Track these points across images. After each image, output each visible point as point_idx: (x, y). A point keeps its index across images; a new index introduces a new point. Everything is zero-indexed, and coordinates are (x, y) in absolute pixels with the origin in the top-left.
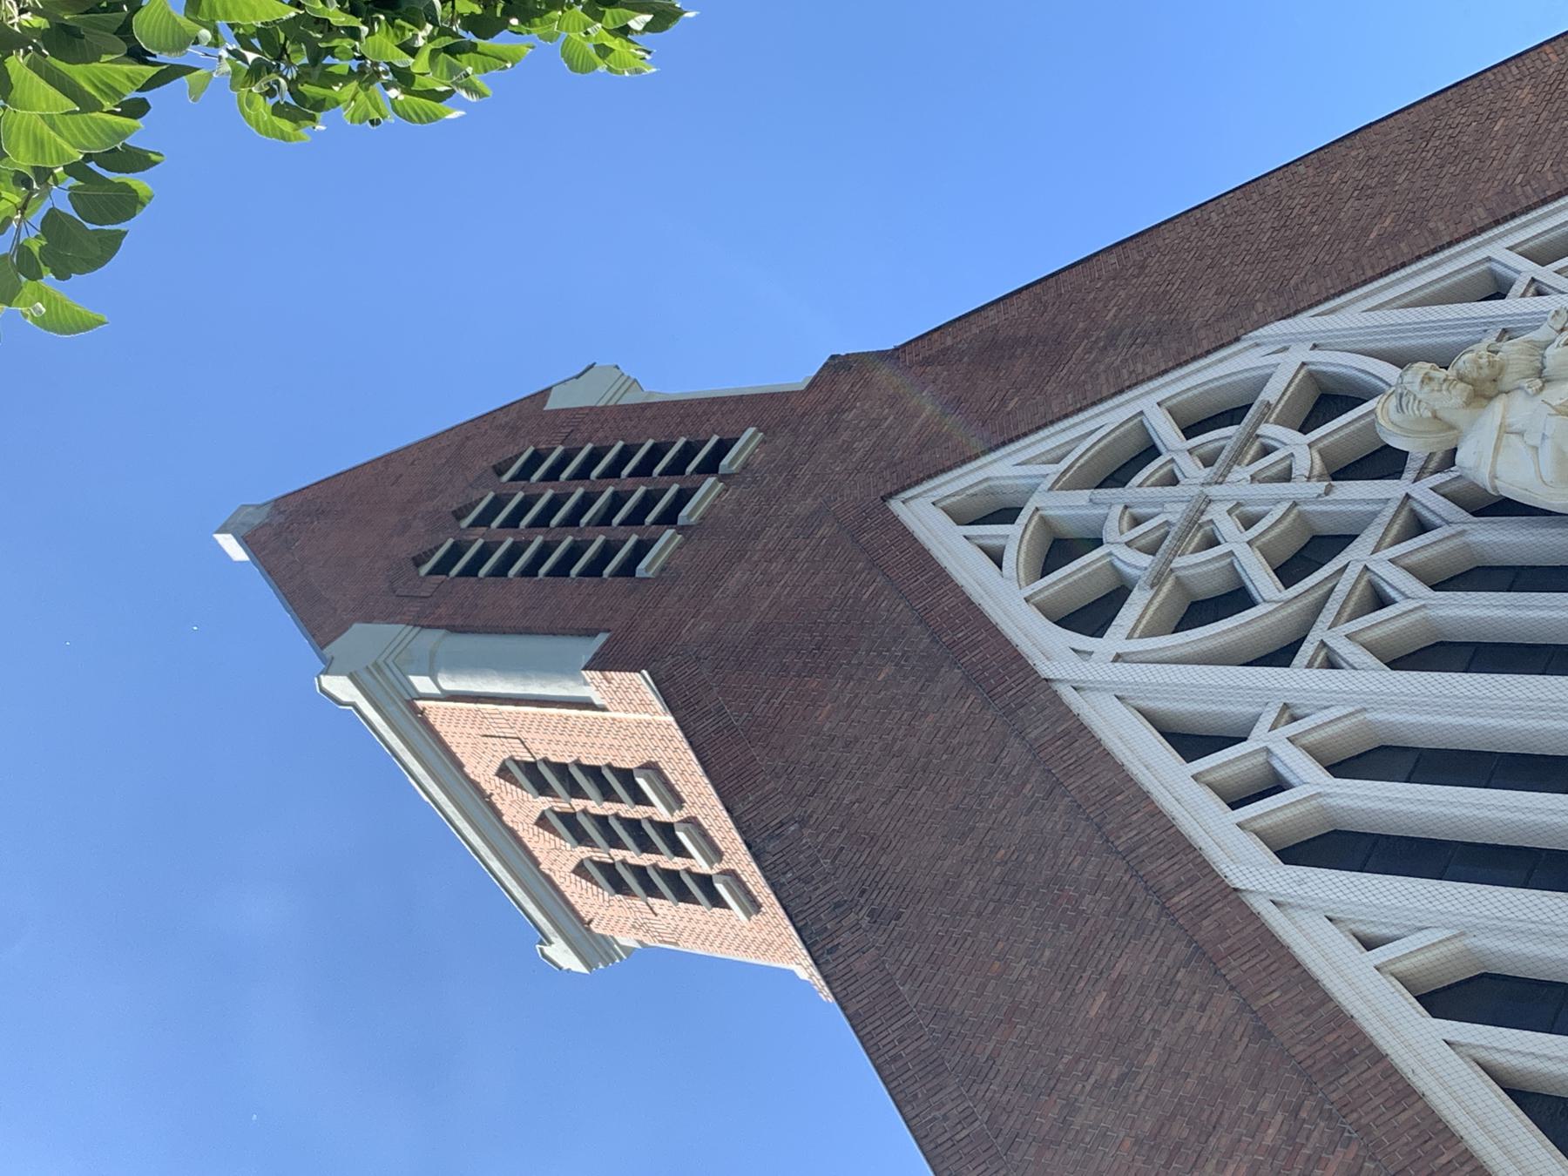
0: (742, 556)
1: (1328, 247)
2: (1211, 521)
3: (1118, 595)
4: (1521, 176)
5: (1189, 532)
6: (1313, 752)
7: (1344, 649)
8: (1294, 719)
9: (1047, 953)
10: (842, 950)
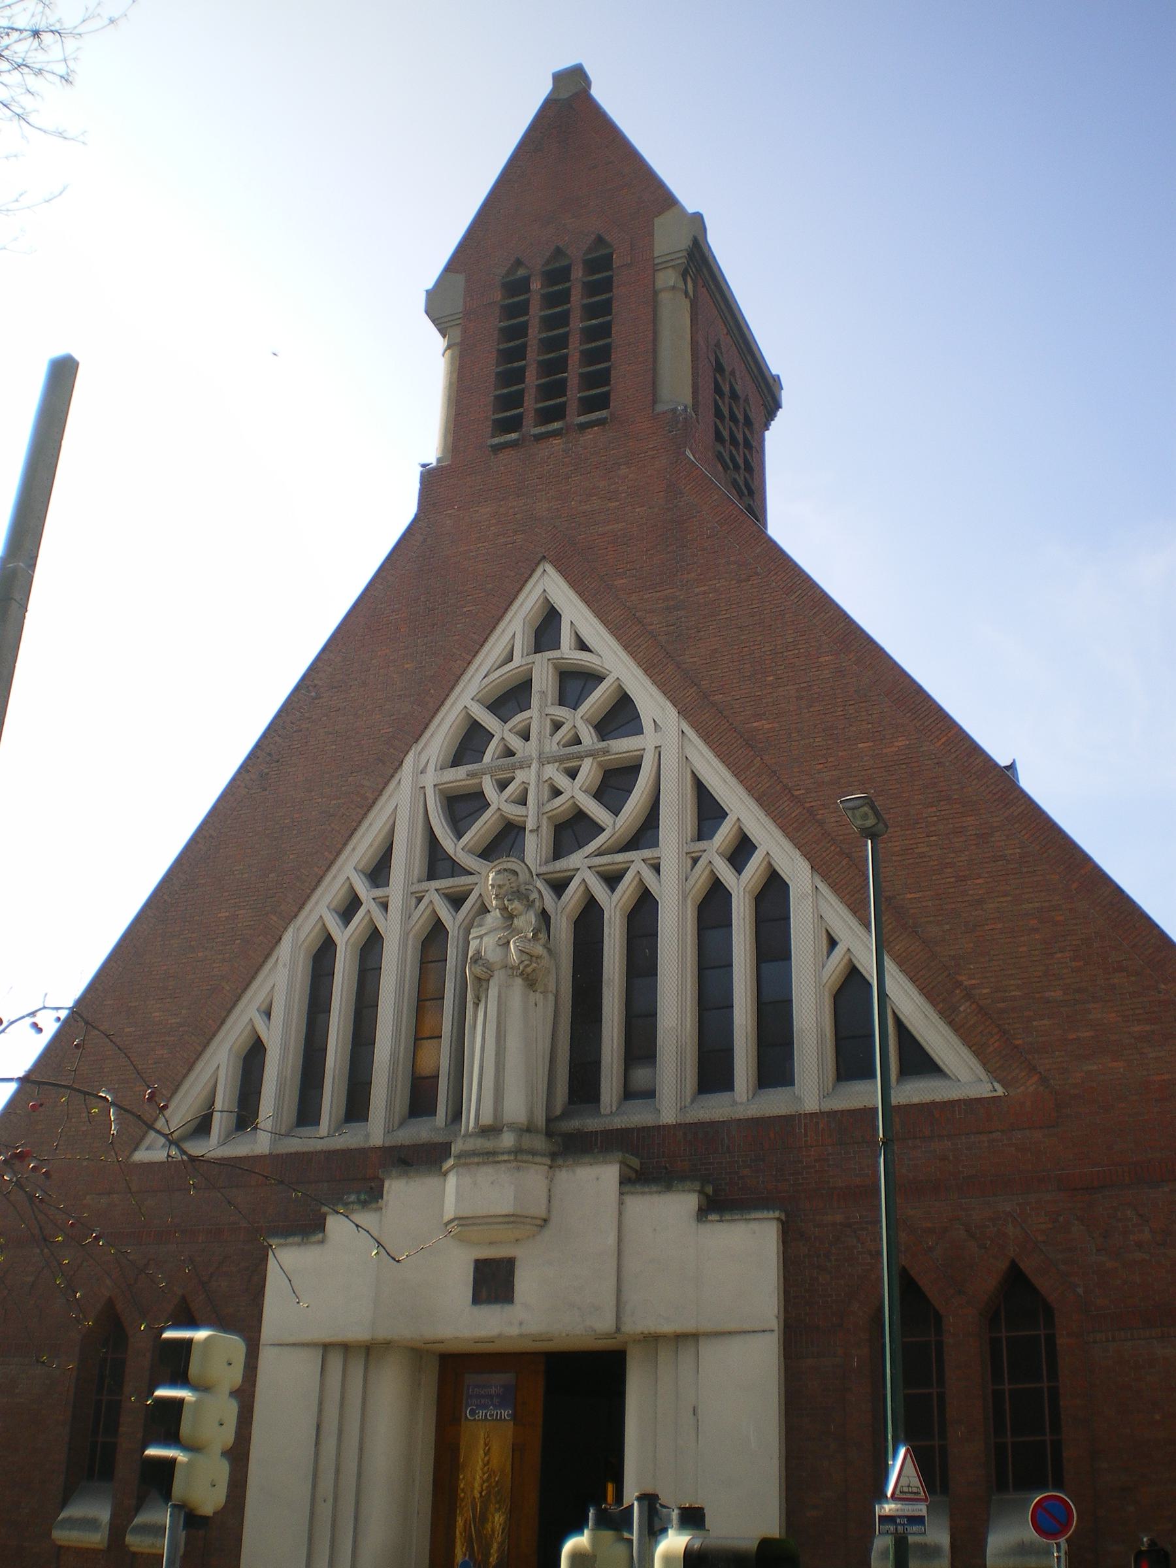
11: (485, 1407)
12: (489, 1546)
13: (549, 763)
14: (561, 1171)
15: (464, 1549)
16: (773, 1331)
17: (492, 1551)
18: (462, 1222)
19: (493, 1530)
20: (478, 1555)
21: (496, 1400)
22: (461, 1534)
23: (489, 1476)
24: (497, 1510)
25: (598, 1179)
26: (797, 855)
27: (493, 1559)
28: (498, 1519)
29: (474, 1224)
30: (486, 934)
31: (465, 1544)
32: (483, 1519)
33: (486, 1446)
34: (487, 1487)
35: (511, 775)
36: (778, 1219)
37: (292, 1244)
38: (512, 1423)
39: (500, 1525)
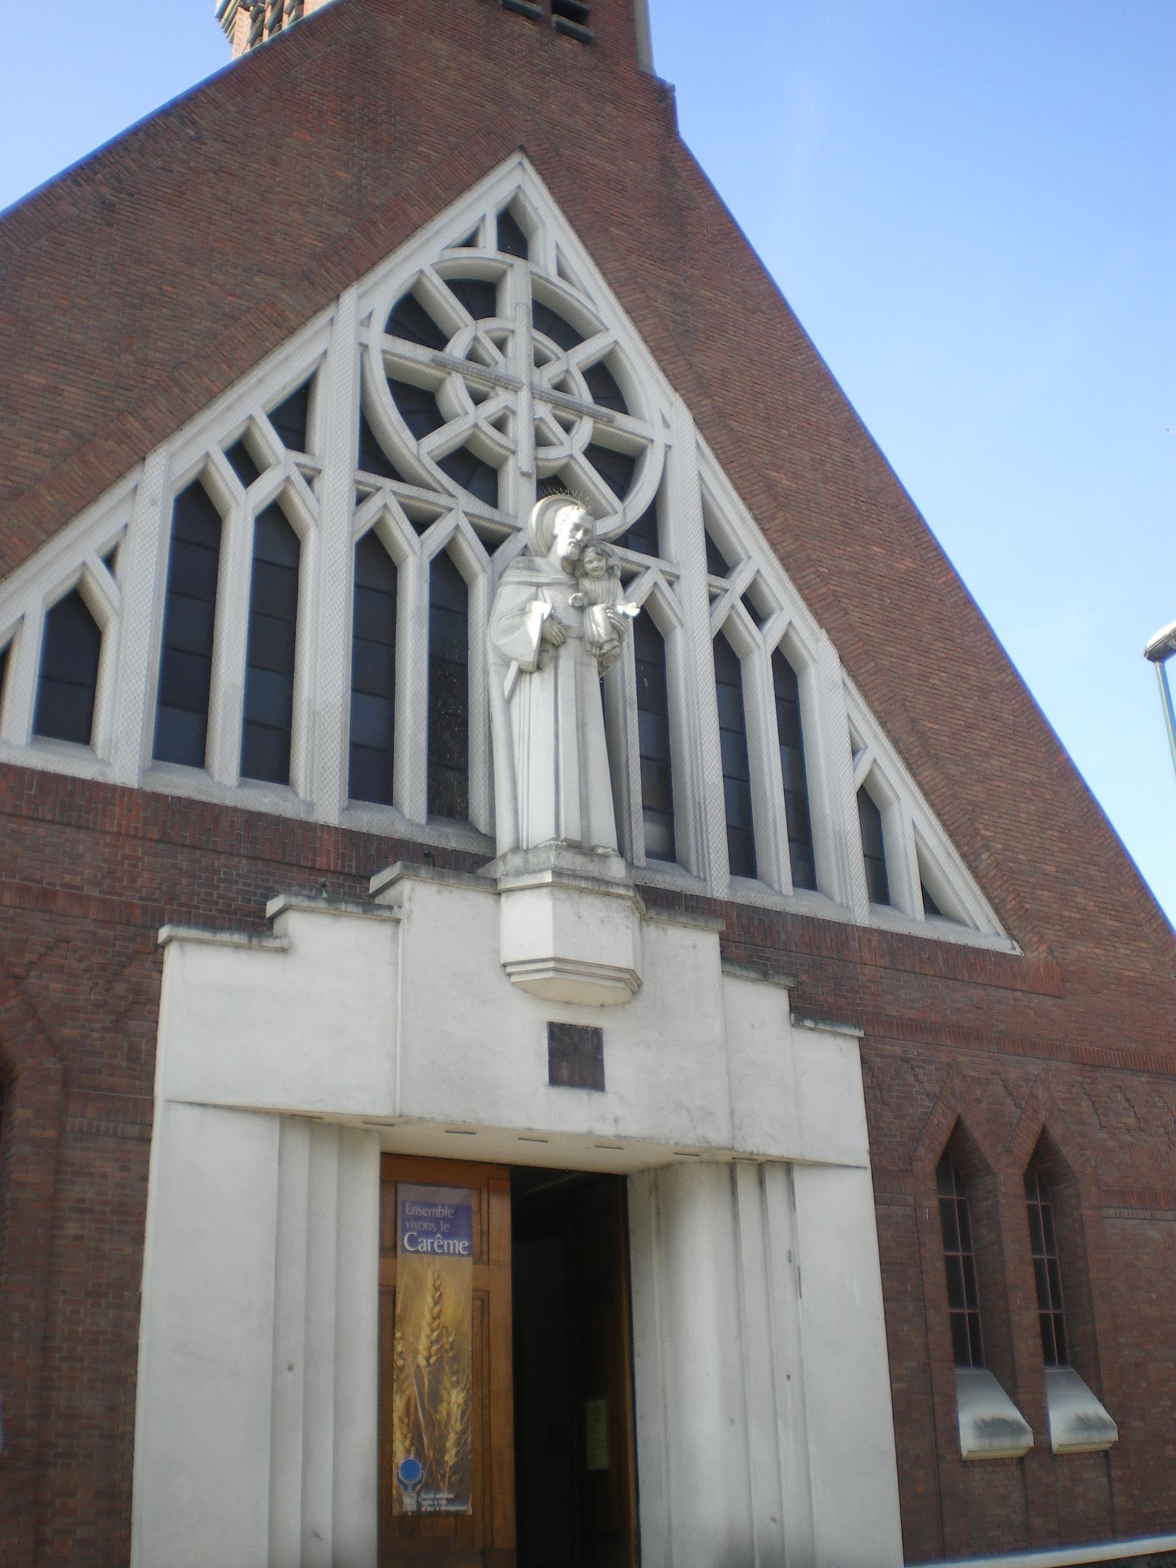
0: (464, 46)
1: (765, 443)
2: (498, 395)
3: (436, 337)
4: (826, 571)
5: (486, 381)
6: (785, 638)
7: (723, 606)
8: (671, 584)
9: (78, 337)
10: (76, 189)
11: (429, 1234)
12: (443, 1437)
13: (540, 399)
14: (648, 925)
15: (408, 1442)
16: (866, 1168)
17: (448, 1445)
18: (558, 965)
19: (449, 1414)
20: (429, 1452)
21: (444, 1227)
22: (401, 1420)
23: (440, 1337)
24: (456, 1384)
25: (694, 947)
26: (823, 635)
27: (450, 1457)
28: (455, 1398)
29: (577, 973)
30: (548, 584)
31: (409, 1436)
32: (436, 1397)
33: (436, 1292)
34: (438, 1350)
35: (486, 389)
36: (860, 1039)
37: (224, 945)
38: (469, 1260)
39: (459, 1406)
